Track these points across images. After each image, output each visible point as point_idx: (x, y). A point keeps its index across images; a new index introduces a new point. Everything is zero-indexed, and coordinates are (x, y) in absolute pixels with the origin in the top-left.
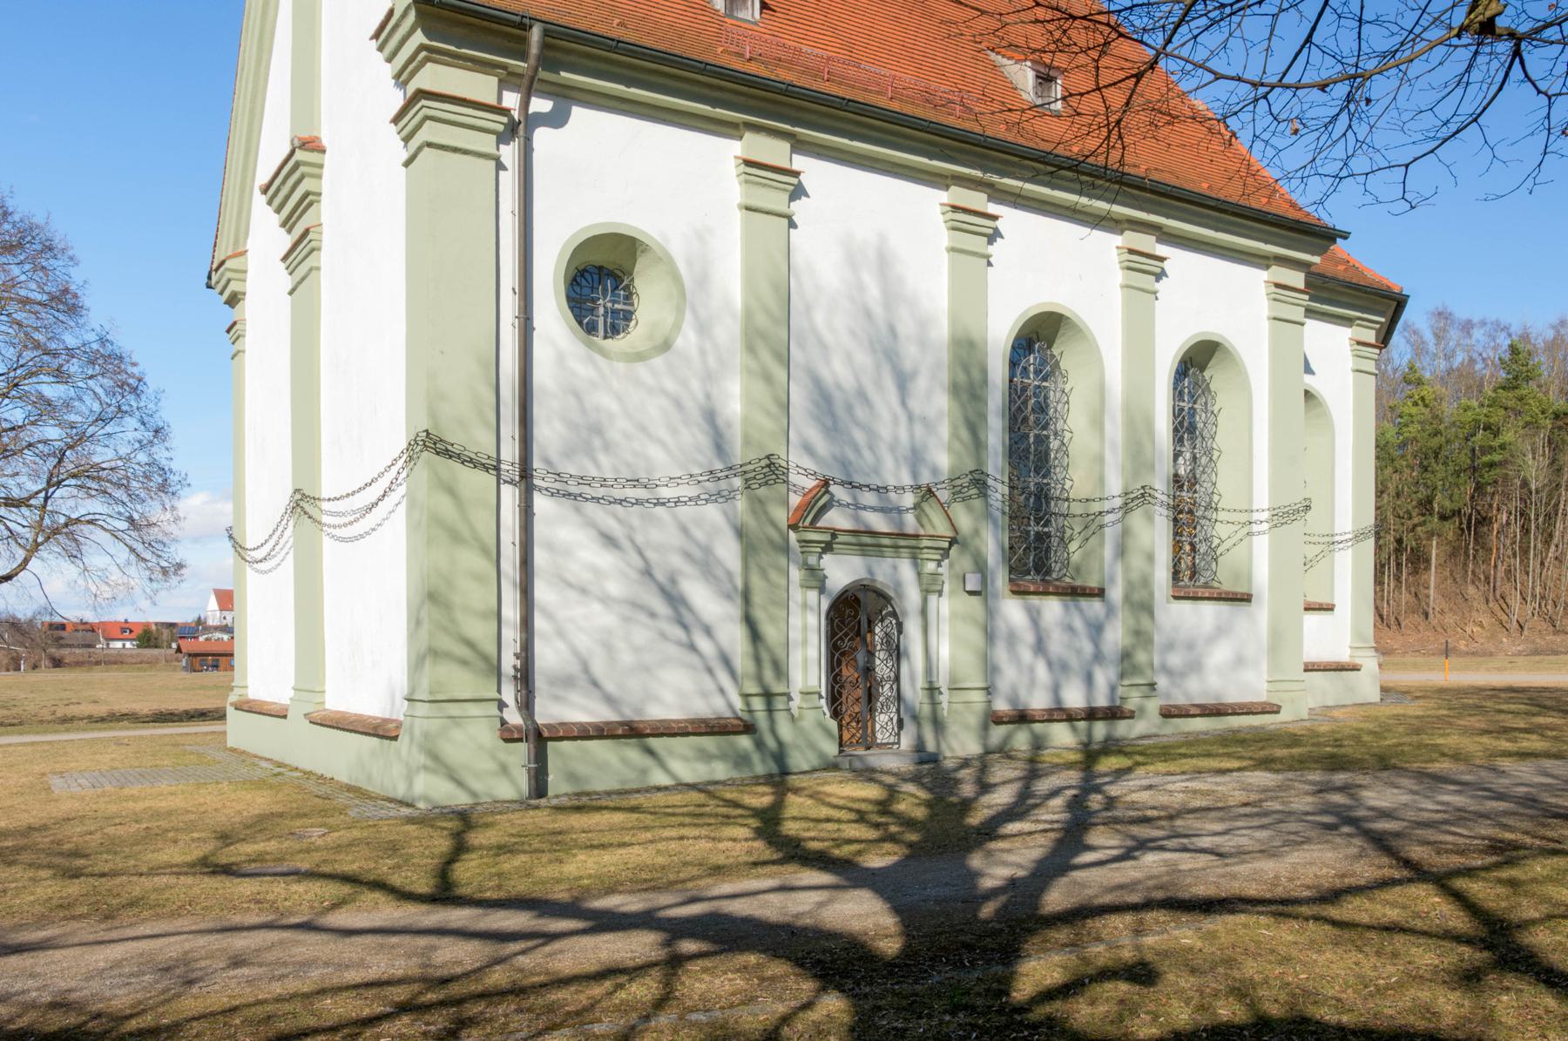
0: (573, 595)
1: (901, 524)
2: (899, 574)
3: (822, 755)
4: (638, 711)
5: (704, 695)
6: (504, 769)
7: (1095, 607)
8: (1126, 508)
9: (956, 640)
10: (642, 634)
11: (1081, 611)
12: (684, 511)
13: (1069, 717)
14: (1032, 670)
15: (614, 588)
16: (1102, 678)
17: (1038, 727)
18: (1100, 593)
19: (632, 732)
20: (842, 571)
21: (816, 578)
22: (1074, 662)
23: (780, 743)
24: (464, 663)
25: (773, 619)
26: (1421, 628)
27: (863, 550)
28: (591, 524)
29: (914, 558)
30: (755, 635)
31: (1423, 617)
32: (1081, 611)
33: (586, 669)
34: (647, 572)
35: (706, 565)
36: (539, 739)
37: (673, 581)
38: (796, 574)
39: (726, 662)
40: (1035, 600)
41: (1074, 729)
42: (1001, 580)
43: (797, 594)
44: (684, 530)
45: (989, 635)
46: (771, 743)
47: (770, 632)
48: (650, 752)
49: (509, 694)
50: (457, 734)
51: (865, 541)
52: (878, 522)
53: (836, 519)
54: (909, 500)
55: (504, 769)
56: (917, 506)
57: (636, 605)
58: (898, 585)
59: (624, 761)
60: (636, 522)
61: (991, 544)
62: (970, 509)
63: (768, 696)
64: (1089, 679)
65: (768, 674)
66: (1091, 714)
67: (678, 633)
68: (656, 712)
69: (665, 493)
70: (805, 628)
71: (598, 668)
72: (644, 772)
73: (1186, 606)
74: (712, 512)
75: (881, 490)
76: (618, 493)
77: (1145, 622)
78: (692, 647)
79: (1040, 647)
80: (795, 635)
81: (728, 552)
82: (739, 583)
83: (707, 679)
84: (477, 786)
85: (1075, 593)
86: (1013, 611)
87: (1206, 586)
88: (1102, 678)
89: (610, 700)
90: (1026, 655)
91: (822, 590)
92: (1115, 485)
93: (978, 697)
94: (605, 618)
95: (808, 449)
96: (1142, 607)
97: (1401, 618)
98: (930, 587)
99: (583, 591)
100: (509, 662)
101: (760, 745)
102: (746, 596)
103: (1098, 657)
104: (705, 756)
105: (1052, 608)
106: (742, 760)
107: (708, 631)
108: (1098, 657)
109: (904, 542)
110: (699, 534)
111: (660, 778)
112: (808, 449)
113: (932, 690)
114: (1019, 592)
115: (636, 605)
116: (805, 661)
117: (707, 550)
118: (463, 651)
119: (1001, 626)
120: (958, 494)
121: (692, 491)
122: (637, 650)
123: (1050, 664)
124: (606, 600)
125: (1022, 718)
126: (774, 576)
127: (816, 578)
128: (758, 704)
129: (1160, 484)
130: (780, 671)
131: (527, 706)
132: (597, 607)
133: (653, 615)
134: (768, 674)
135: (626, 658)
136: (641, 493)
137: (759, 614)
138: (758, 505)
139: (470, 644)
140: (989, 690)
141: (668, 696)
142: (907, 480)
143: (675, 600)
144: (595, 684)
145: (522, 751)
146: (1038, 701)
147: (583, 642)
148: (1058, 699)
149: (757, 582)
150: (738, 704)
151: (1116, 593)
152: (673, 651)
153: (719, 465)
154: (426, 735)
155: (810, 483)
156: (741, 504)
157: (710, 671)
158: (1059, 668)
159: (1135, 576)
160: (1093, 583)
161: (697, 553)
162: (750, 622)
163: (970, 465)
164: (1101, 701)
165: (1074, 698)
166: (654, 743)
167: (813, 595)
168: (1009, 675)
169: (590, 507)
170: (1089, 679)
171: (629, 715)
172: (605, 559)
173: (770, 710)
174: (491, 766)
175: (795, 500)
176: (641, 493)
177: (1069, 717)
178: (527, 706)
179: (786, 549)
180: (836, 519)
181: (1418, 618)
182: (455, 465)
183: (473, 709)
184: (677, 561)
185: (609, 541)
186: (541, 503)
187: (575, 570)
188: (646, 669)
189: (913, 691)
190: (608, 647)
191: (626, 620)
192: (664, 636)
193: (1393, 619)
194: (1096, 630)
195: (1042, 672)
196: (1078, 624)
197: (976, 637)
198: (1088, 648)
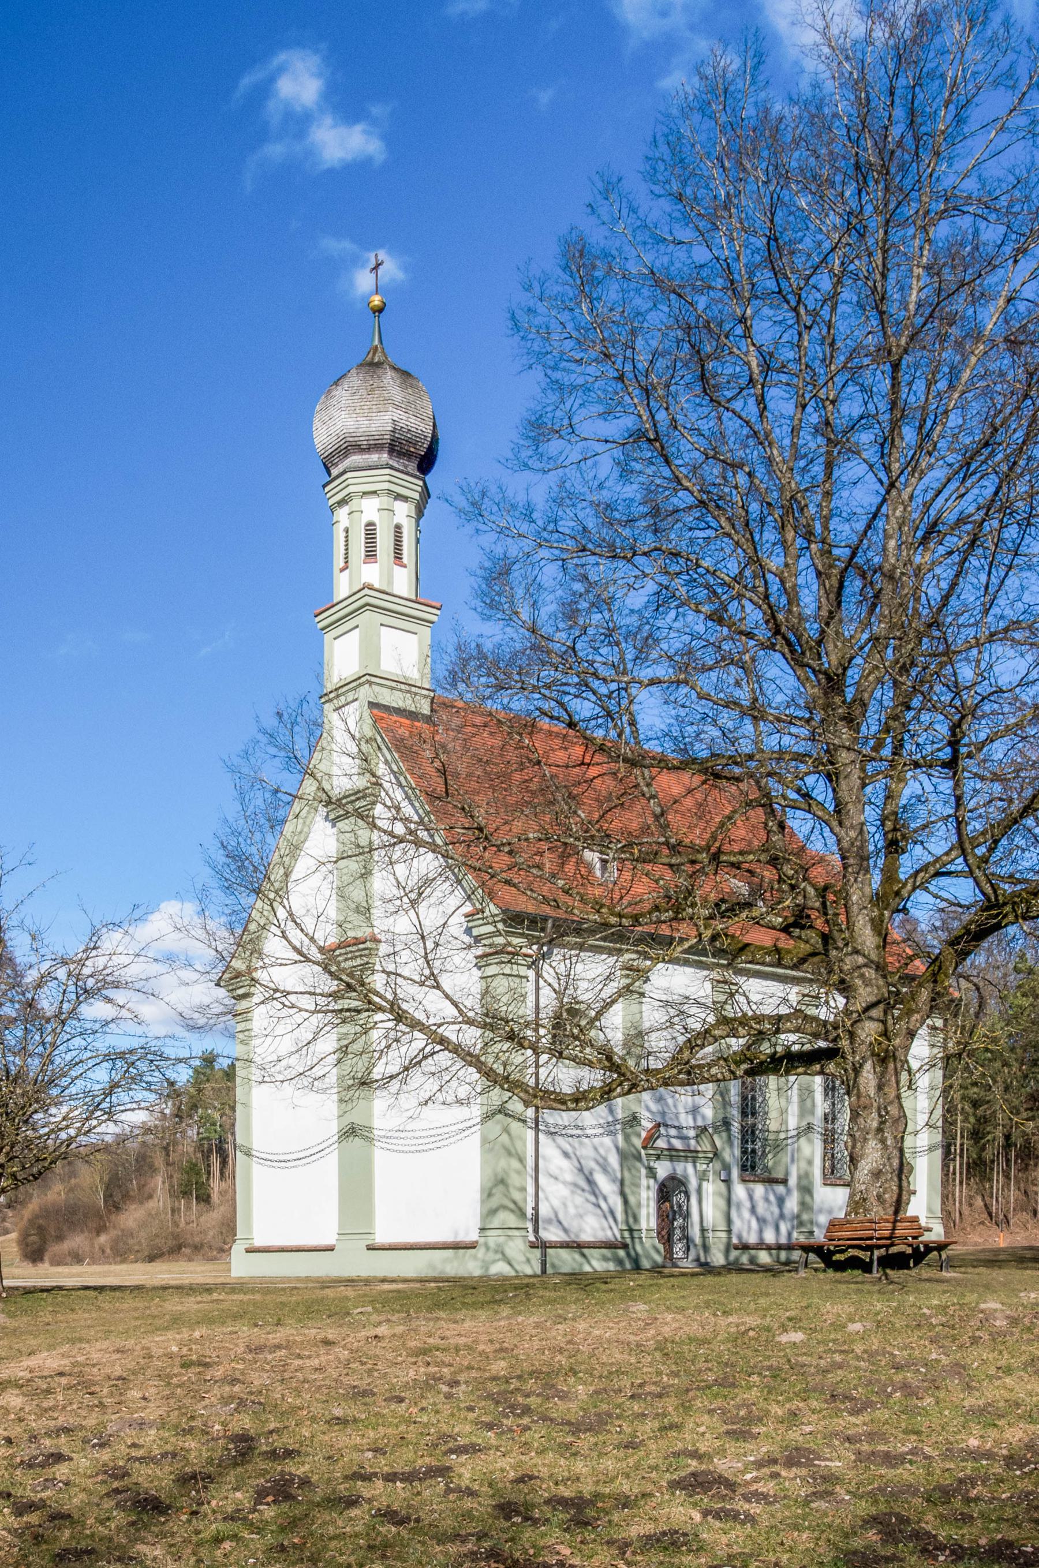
0: (552, 1180)
1: (689, 1145)
2: (688, 1170)
3: (655, 1262)
4: (577, 1236)
5: (603, 1229)
6: (528, 1261)
7: (780, 1189)
8: (798, 1136)
9: (715, 1206)
10: (579, 1199)
11: (773, 1191)
12: (596, 1140)
13: (769, 1248)
14: (749, 1222)
15: (569, 1177)
16: (784, 1228)
17: (753, 1252)
18: (784, 1182)
19: (579, 1246)
20: (663, 1169)
21: (652, 1173)
22: (769, 1217)
23: (637, 1254)
24: (512, 1211)
25: (633, 1193)
26: (1029, 1226)
27: (671, 1159)
28: (559, 1147)
29: (694, 1162)
30: (626, 1202)
31: (1031, 1214)
32: (773, 1191)
33: (556, 1216)
34: (581, 1170)
35: (605, 1168)
36: (542, 1246)
37: (591, 1173)
38: (643, 1171)
39: (612, 1213)
40: (751, 1185)
41: (771, 1255)
42: (735, 1173)
43: (644, 1182)
44: (596, 1149)
45: (729, 1201)
46: (633, 1253)
47: (632, 1200)
48: (584, 1255)
49: (530, 1226)
50: (511, 1244)
51: (672, 1154)
52: (678, 1144)
53: (661, 1143)
54: (692, 1133)
55: (528, 1261)
56: (697, 1136)
57: (576, 1185)
58: (686, 1177)
59: (574, 1259)
60: (577, 1145)
61: (732, 1154)
62: (721, 1137)
63: (631, 1231)
64: (777, 1229)
65: (631, 1220)
66: (779, 1247)
67: (592, 1199)
68: (586, 1237)
69: (589, 1132)
70: (648, 1199)
71: (561, 1216)
72: (581, 1265)
73: (829, 1189)
74: (607, 1141)
75: (679, 1128)
76: (570, 1132)
77: (808, 1199)
78: (599, 1206)
79: (753, 1210)
80: (644, 1202)
81: (614, 1160)
82: (619, 1175)
83: (603, 1221)
84: (518, 1268)
85: (771, 1181)
86: (740, 1191)
87: (840, 1178)
88: (784, 1228)
89: (566, 1231)
90: (746, 1214)
91: (655, 1177)
92: (793, 1122)
93: (724, 1235)
94: (564, 1191)
95: (648, 1109)
96: (806, 1189)
97: (1010, 1216)
98: (702, 1177)
99: (556, 1179)
100: (529, 1211)
101: (628, 1254)
102: (622, 1183)
103: (782, 1216)
104: (605, 1259)
105: (759, 1189)
106: (620, 1262)
107: (605, 1199)
108: (782, 1216)
109: (691, 1155)
110: (602, 1151)
111: (587, 1268)
112: (648, 1109)
113: (703, 1230)
114: (744, 1181)
115: (576, 1185)
116: (648, 1215)
117: (605, 1159)
118: (512, 1206)
119: (734, 1198)
120: (716, 1129)
121: (601, 1131)
122: (576, 1207)
123: (758, 1219)
124: (565, 1183)
125: (745, 1247)
126: (634, 1171)
127: (652, 1173)
128: (626, 1234)
129: (817, 1120)
130: (636, 1219)
131: (536, 1230)
132: (561, 1186)
133: (583, 1190)
134: (631, 1220)
135: (572, 1211)
136: (579, 1132)
137: (627, 1190)
138: (627, 1138)
139: (515, 1203)
140: (729, 1231)
141: (588, 1230)
142: (691, 1123)
143: (590, 1181)
144: (560, 1223)
145: (538, 1253)
146: (752, 1239)
147: (556, 1203)
148: (761, 1239)
149: (627, 1174)
150: (618, 1236)
151: (793, 1181)
152: (591, 1207)
153: (610, 1119)
154: (499, 1245)
155: (650, 1125)
156: (620, 1137)
157: (605, 1217)
158: (762, 1221)
159: (802, 1172)
160: (780, 1175)
161: (601, 1161)
162: (623, 1194)
163: (721, 1116)
164: (783, 1240)
165: (770, 1237)
166: (586, 1251)
167: (652, 1182)
168: (737, 1225)
169: (560, 1140)
170: (777, 1229)
171: (573, 1238)
172: (565, 1163)
173: (632, 1238)
174: (524, 1259)
175: (644, 1134)
176: (579, 1132)
177: (769, 1248)
178: (536, 1230)
179: (639, 1158)
180: (661, 1143)
181: (1026, 1216)
182: (510, 1120)
183: (516, 1233)
184: (593, 1165)
185: (566, 1155)
186: (541, 1136)
187: (555, 1171)
188: (581, 1216)
189: (695, 1233)
190: (565, 1205)
191: (573, 1192)
192: (587, 1200)
193: (1001, 1217)
194: (781, 1201)
195: (754, 1224)
196: (772, 1198)
197: (722, 1203)
198: (776, 1210)
